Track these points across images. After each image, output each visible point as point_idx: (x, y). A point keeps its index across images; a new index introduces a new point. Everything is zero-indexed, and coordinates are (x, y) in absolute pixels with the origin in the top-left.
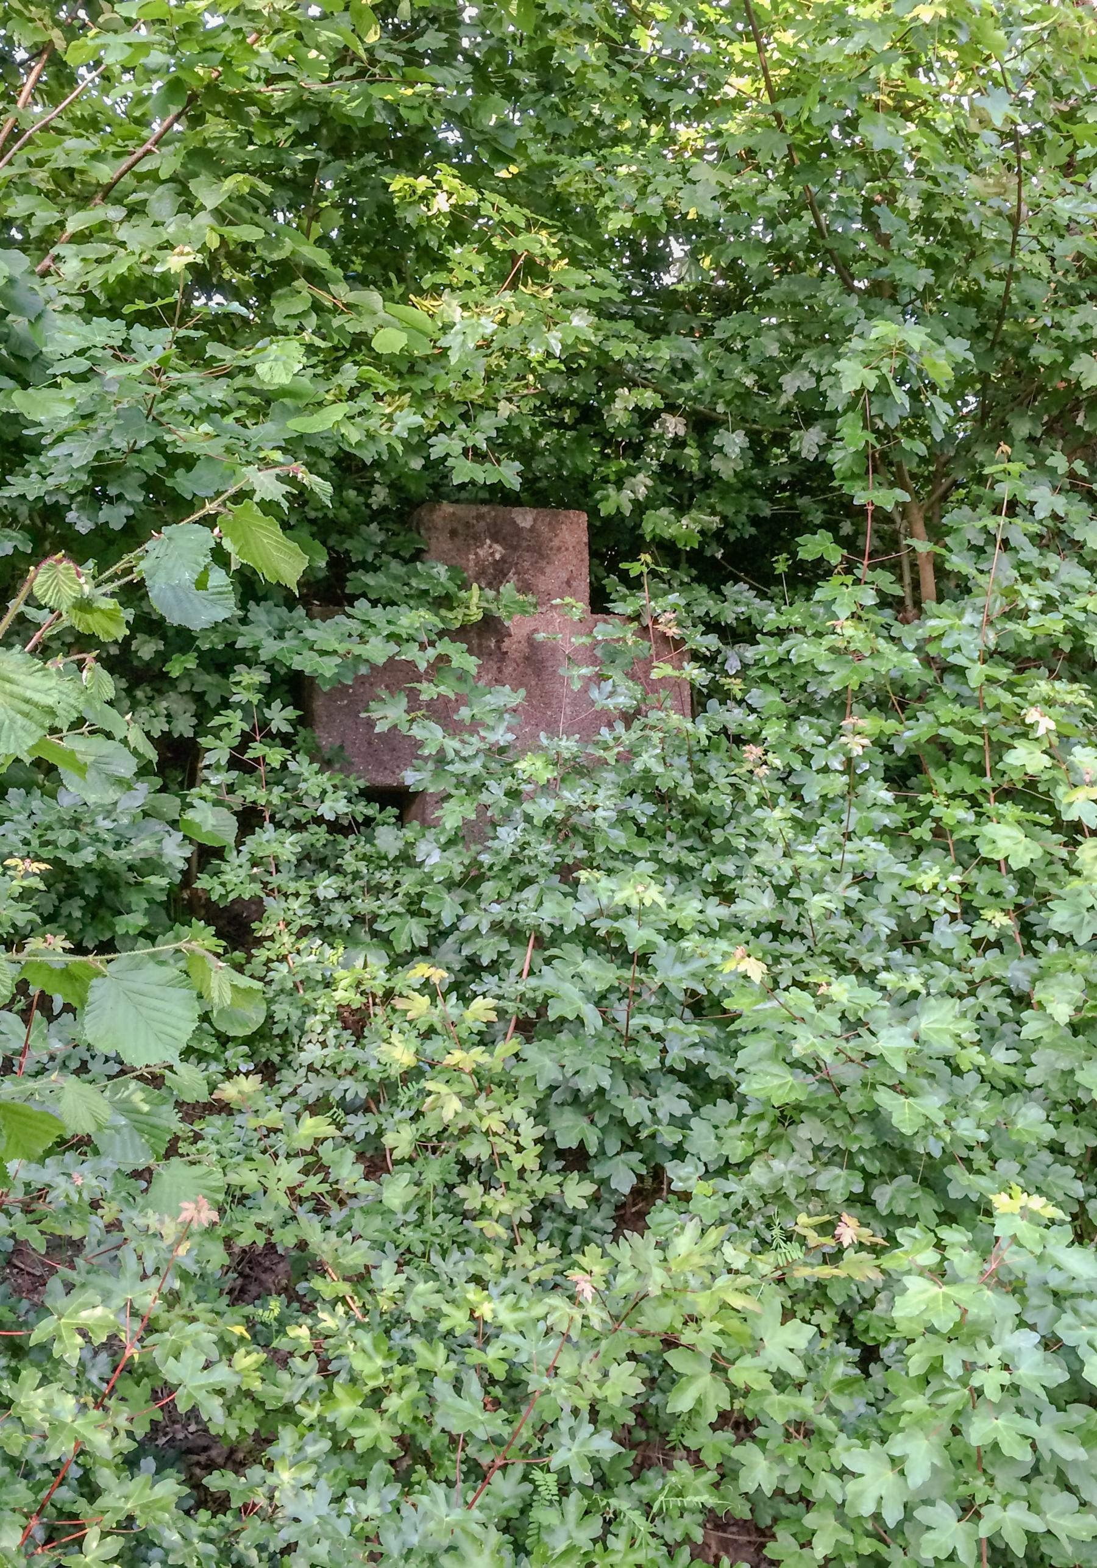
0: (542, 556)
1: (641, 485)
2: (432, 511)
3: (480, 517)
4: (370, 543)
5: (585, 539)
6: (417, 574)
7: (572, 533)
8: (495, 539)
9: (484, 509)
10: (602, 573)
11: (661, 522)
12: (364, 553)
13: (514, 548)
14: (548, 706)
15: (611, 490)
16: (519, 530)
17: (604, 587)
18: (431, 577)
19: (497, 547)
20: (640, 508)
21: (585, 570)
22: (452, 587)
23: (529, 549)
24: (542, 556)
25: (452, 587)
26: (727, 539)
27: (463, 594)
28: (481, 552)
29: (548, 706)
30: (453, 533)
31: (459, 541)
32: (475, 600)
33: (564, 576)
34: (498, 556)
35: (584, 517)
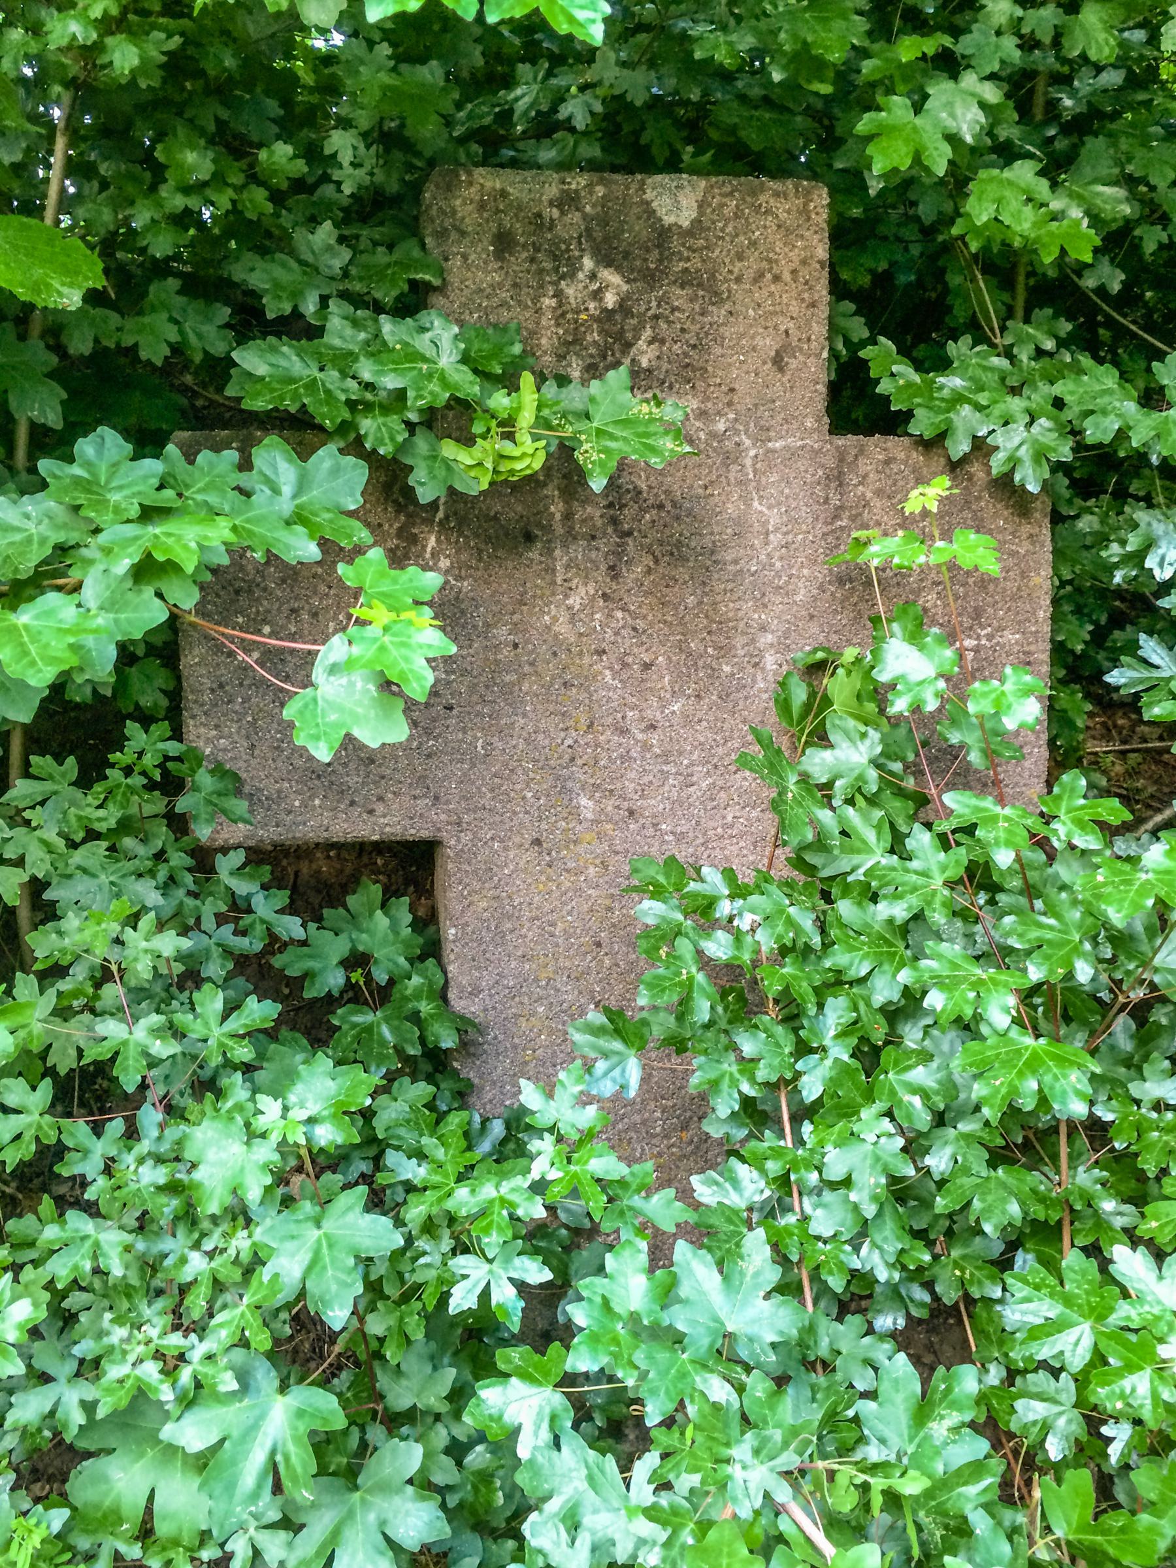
0: (717, 298)
1: (961, 109)
2: (449, 188)
3: (568, 201)
4: (310, 269)
5: (822, 252)
6: (377, 348)
7: (784, 236)
8: (606, 259)
9: (578, 181)
10: (858, 329)
11: (1015, 206)
12: (296, 295)
13: (651, 278)
14: (725, 651)
15: (898, 106)
16: (663, 234)
17: (864, 364)
18: (417, 356)
19: (611, 277)
20: (967, 165)
21: (819, 330)
22: (468, 385)
23: (686, 280)
24: (717, 298)
25: (468, 385)
26: (1136, 247)
27: (500, 401)
28: (571, 291)
29: (725, 651)
30: (504, 243)
31: (518, 261)
32: (526, 418)
33: (768, 344)
34: (610, 300)
35: (821, 198)
